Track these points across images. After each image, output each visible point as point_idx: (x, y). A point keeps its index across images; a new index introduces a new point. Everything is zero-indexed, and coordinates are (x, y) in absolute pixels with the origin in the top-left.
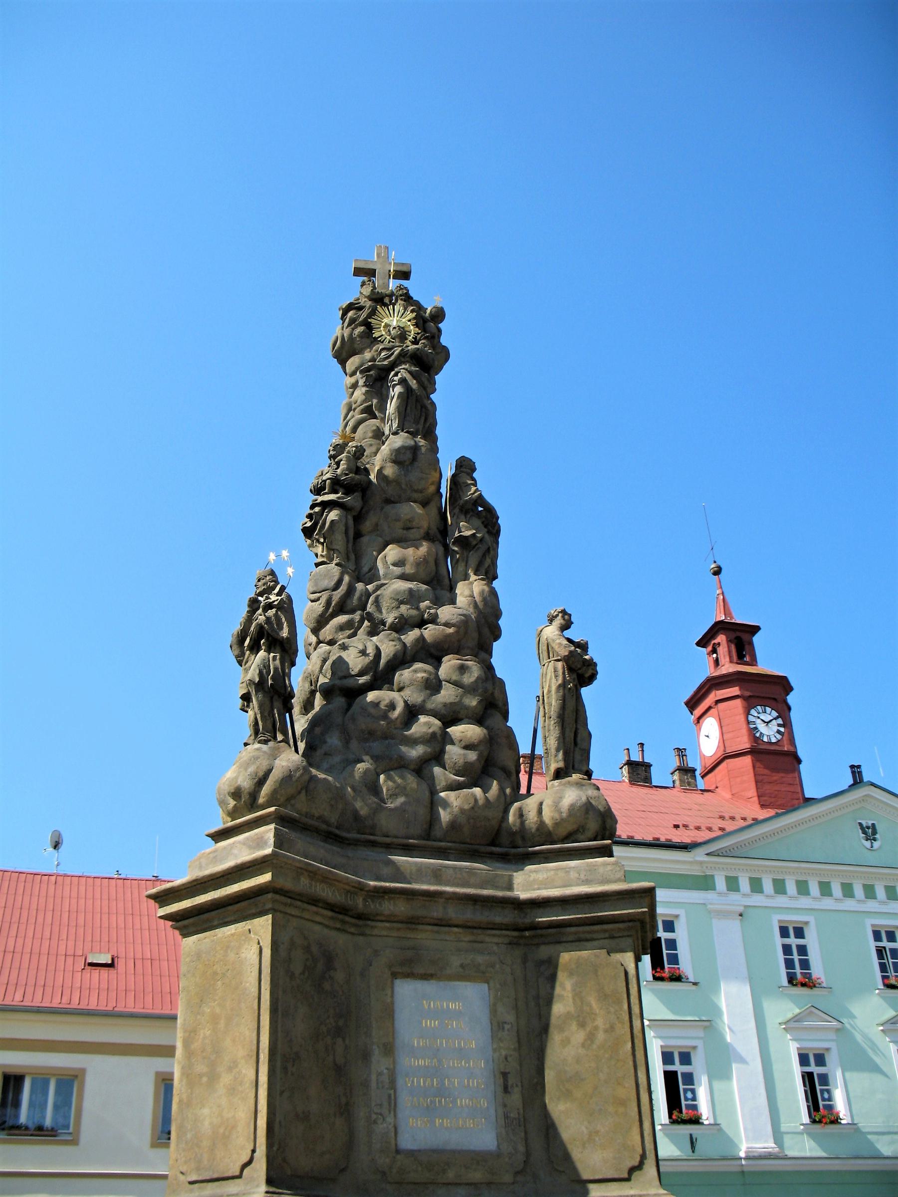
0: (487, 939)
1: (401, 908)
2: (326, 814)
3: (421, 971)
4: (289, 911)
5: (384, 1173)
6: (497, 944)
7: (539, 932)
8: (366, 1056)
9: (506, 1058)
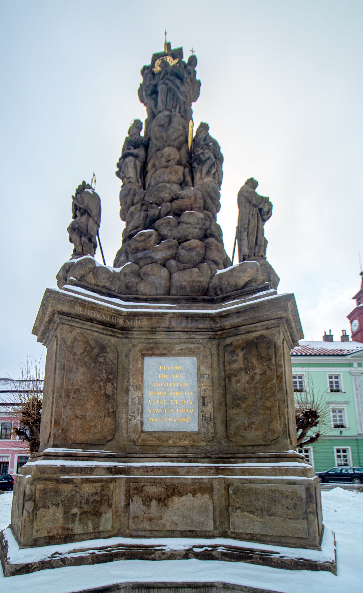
0: (197, 337)
1: (145, 323)
2: (107, 285)
3: (158, 352)
4: (73, 324)
5: (134, 442)
6: (202, 339)
7: (226, 331)
8: (127, 391)
9: (205, 390)
